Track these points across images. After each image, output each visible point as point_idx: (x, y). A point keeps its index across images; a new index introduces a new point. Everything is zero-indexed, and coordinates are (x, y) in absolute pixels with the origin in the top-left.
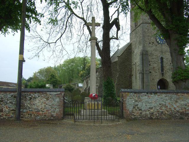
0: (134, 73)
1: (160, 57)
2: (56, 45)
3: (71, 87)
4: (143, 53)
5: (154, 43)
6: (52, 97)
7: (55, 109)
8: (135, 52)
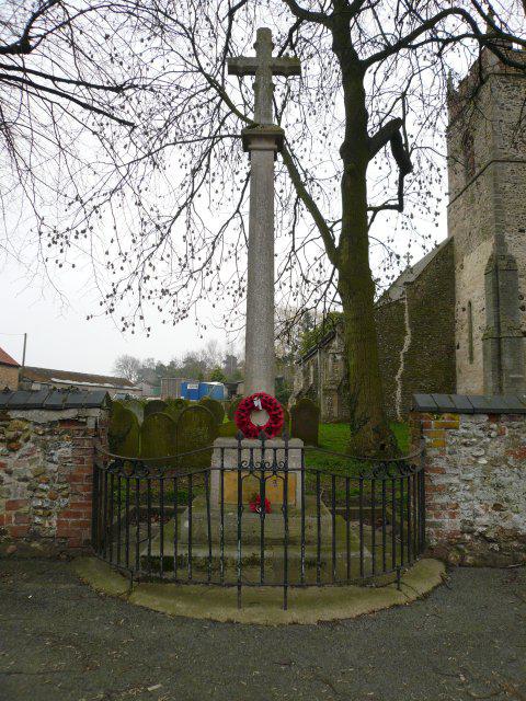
0: (461, 338)
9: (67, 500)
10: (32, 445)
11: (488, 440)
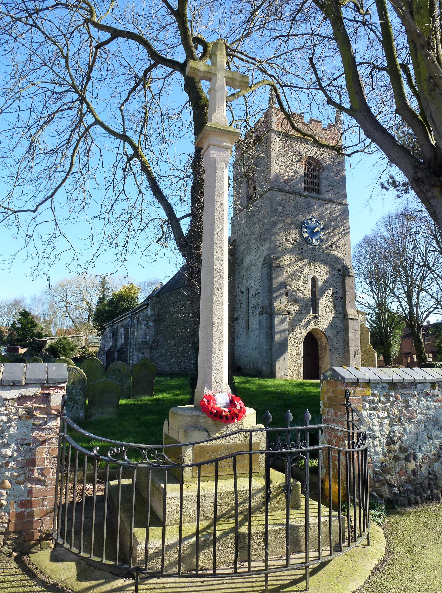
2: (38, 220)
3: (69, 343)
8: (247, 261)
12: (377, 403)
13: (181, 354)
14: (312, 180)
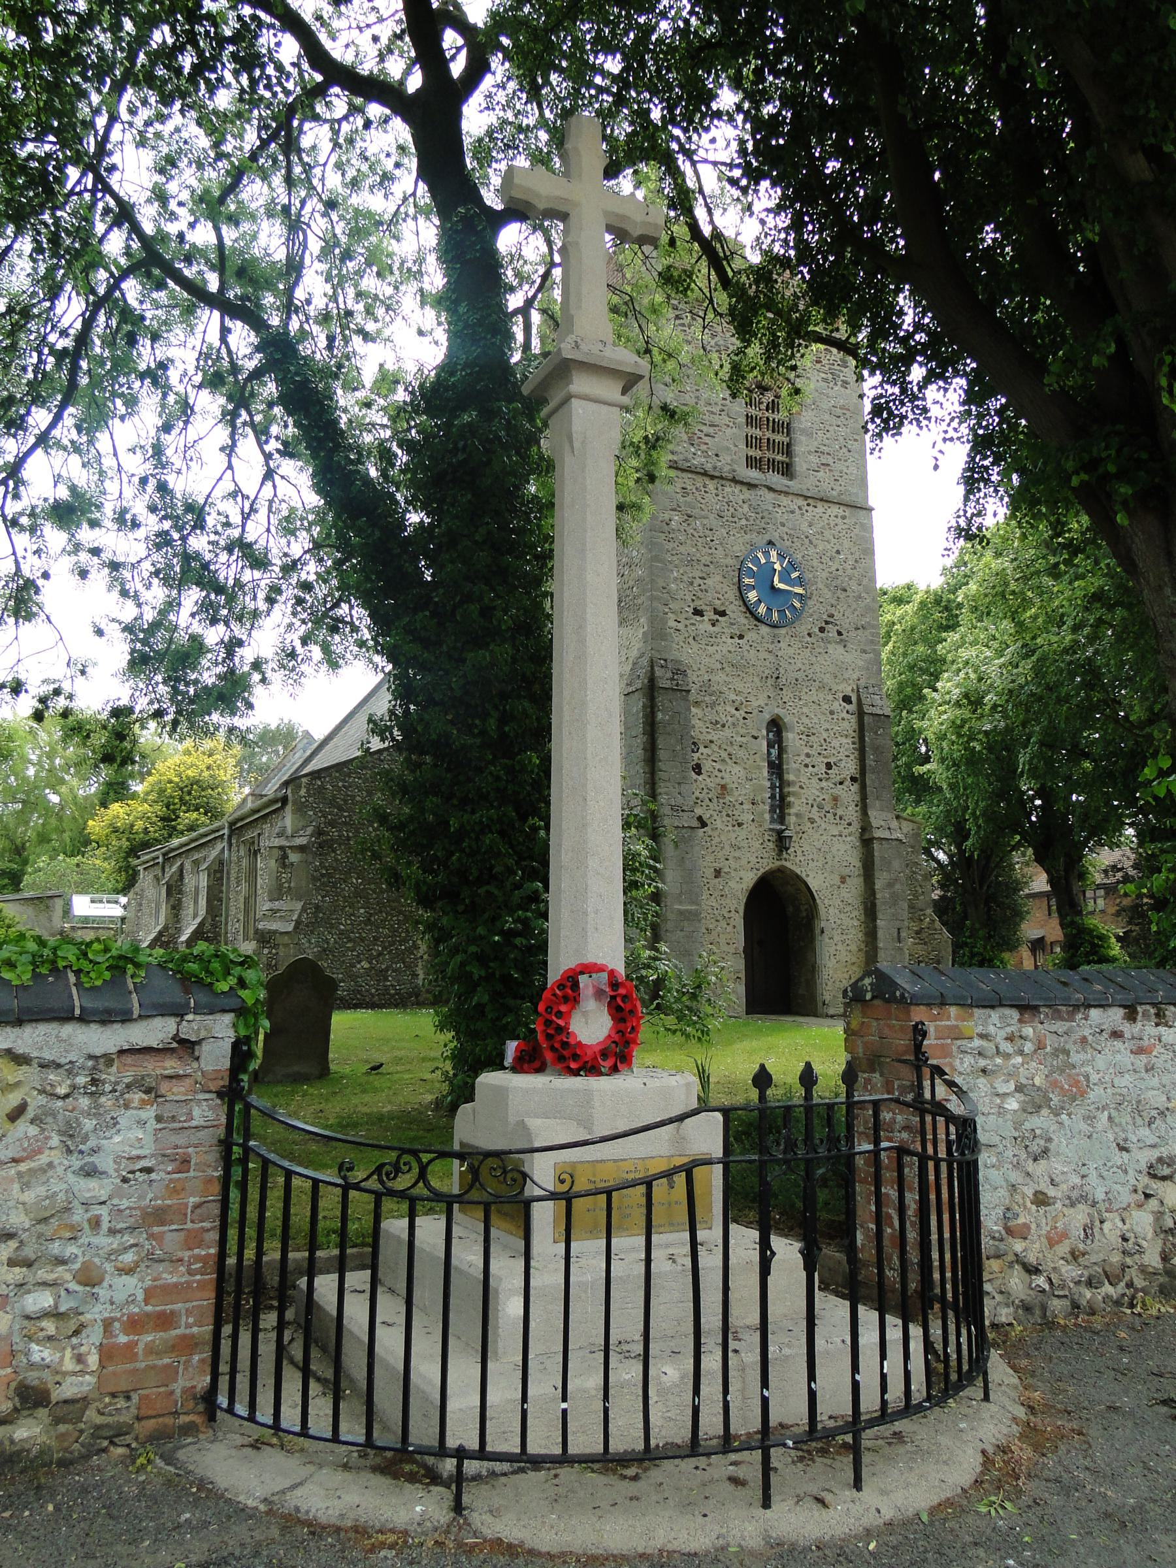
1: (767, 717)
4: (652, 680)
5: (723, 614)
6: (36, 1102)
7: (89, 1279)
9: (131, 1281)
10: (33, 1131)
11: (1019, 1059)
12: (992, 1058)
13: (384, 948)
14: (769, 434)
